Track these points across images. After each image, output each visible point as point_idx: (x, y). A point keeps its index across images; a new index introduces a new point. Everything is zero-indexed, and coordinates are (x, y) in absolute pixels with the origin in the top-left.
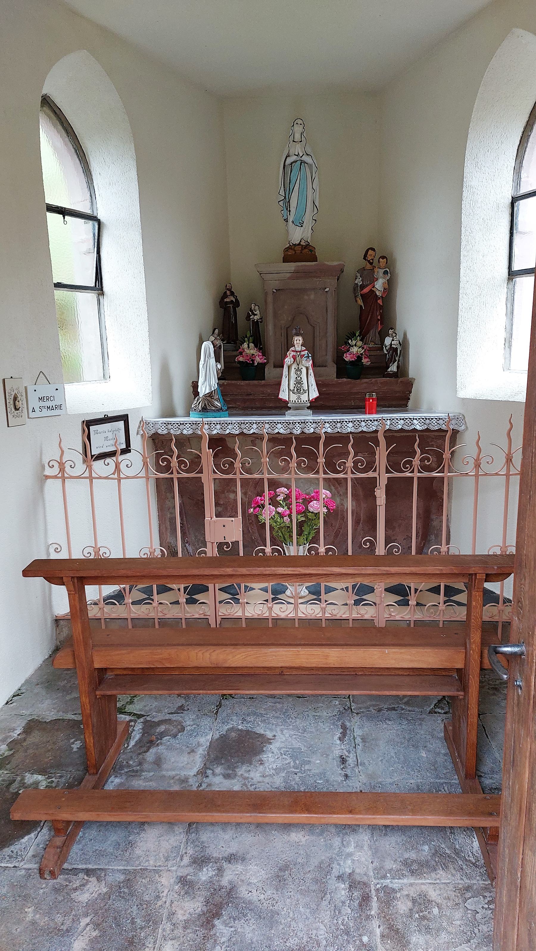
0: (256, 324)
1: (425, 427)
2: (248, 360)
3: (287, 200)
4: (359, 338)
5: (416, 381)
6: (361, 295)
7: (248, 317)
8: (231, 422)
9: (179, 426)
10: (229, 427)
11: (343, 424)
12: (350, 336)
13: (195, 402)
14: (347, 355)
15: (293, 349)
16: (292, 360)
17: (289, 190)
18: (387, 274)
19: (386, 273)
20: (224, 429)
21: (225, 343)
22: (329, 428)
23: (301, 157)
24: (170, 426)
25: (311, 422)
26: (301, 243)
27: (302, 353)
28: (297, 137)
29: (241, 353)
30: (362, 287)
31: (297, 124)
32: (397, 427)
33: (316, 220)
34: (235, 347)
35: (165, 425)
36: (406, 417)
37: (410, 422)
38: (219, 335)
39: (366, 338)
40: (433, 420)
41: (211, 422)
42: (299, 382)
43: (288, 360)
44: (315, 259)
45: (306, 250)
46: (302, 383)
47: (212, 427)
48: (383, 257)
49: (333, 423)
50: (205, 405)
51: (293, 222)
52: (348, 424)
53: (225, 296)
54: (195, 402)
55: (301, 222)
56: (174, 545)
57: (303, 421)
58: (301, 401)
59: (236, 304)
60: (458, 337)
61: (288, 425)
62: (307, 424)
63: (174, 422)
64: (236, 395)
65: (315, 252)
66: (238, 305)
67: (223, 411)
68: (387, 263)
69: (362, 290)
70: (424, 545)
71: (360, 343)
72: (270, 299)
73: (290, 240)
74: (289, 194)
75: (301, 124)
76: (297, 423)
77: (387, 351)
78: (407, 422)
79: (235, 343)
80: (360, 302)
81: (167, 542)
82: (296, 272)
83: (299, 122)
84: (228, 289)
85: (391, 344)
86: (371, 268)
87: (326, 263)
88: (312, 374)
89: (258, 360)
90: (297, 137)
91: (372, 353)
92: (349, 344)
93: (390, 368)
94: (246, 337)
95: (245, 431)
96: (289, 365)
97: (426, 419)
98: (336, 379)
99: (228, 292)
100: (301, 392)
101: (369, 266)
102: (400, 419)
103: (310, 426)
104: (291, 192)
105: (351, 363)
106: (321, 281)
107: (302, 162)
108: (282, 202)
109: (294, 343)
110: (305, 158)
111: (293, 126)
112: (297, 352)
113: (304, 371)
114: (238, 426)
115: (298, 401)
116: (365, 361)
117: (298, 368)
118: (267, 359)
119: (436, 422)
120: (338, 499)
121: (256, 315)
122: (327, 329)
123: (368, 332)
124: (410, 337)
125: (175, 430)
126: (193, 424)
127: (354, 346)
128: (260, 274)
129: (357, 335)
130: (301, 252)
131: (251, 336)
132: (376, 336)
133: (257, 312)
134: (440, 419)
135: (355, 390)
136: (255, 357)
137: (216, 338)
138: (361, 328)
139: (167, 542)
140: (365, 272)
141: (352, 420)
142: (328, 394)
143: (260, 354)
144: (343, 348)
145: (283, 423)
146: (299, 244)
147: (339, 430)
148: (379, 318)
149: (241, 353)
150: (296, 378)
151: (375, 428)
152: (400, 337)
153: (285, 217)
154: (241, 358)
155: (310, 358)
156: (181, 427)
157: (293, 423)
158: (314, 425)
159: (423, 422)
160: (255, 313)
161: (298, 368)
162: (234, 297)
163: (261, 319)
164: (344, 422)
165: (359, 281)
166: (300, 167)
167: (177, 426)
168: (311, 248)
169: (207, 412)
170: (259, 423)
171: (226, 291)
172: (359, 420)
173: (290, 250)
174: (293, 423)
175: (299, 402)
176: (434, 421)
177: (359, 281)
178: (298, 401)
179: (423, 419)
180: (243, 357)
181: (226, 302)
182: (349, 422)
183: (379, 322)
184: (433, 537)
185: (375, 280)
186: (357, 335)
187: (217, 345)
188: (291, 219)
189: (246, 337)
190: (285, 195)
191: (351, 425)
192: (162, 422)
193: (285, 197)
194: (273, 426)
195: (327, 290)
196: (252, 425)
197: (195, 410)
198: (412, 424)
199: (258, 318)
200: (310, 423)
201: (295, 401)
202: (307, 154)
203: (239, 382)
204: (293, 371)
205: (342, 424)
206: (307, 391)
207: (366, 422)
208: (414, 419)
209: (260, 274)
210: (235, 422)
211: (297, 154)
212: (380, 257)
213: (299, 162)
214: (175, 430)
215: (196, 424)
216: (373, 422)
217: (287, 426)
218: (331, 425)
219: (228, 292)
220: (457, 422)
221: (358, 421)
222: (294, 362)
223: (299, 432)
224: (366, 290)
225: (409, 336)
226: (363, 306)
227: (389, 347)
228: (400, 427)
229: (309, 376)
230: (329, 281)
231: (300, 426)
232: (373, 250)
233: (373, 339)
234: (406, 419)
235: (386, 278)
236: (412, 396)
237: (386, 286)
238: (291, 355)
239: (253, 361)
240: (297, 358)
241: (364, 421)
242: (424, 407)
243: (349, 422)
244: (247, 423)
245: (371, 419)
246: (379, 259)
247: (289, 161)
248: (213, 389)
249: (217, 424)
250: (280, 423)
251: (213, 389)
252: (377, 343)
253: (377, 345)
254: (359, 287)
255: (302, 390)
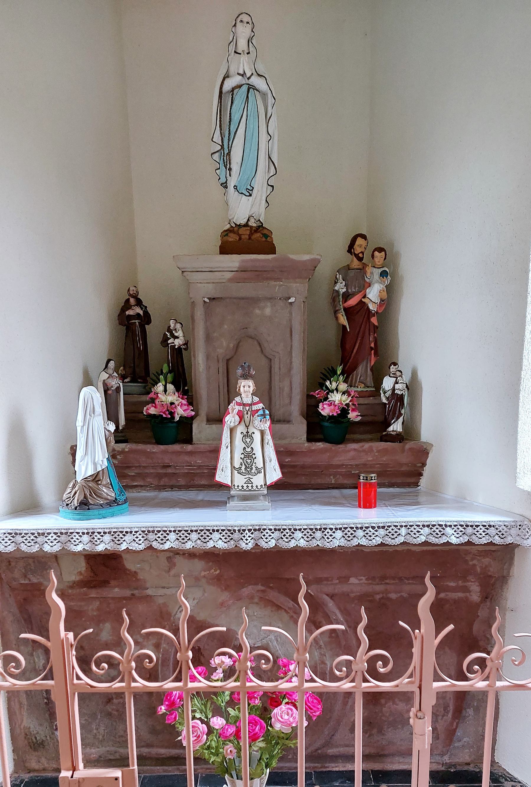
0: (178, 352)
1: (465, 539)
2: (164, 413)
3: (226, 151)
4: (341, 378)
5: (434, 448)
6: (345, 309)
7: (165, 340)
8: (129, 530)
9: (36, 537)
10: (125, 538)
11: (326, 533)
12: (328, 375)
13: (69, 490)
14: (325, 406)
15: (238, 399)
16: (237, 418)
17: (229, 134)
18: (387, 277)
19: (384, 274)
20: (117, 542)
21: (128, 382)
22: (302, 540)
23: (249, 78)
24: (19, 539)
25: (270, 530)
26: (250, 224)
27: (255, 408)
28: (242, 45)
29: (153, 401)
30: (347, 296)
31: (241, 21)
32: (418, 539)
33: (272, 186)
34: (145, 387)
35: (9, 537)
36: (433, 523)
37: (440, 531)
38: (116, 370)
39: (352, 378)
40: (479, 528)
41: (95, 530)
42: (248, 456)
43: (231, 419)
44: (272, 250)
45: (258, 235)
46: (254, 456)
47: (96, 538)
48: (380, 250)
49: (309, 531)
50: (85, 497)
51: (235, 187)
52: (334, 532)
53: (127, 305)
54: (69, 490)
55: (249, 187)
56: (35, 732)
57: (257, 528)
58: (252, 487)
59: (146, 318)
60: (521, 388)
61: (232, 534)
62: (265, 533)
63: (27, 532)
64: (145, 467)
65: (272, 238)
66: (149, 322)
67: (118, 505)
68: (385, 259)
69: (345, 302)
70: (457, 724)
71: (343, 387)
72: (199, 313)
73: (230, 218)
74: (229, 142)
75: (248, 23)
76: (247, 531)
77: (387, 399)
78: (434, 531)
79: (145, 381)
80: (343, 320)
81: (22, 727)
82: (242, 270)
83: (246, 18)
84: (131, 295)
85: (394, 389)
86: (360, 267)
87: (292, 256)
88: (271, 443)
89: (180, 412)
90: (242, 45)
91: (362, 401)
92: (327, 388)
93: (392, 426)
94: (162, 373)
95: (155, 545)
96: (231, 427)
97: (467, 526)
98: (306, 445)
99: (132, 301)
100: (253, 471)
101: (356, 263)
102: (424, 526)
103: (270, 536)
104: (231, 138)
105: (331, 418)
106: (282, 285)
107: (251, 87)
108: (217, 154)
109: (239, 390)
110: (255, 81)
111: (235, 25)
112: (244, 405)
113: (257, 437)
114: (143, 537)
115: (248, 487)
116: (353, 416)
117: (248, 432)
118: (196, 410)
119: (484, 532)
120: (316, 654)
121: (177, 337)
122: (291, 363)
123: (354, 368)
124: (424, 377)
125: (29, 544)
126: (62, 533)
127: (335, 392)
128: (183, 272)
129: (339, 373)
130: (250, 238)
131: (170, 372)
132: (366, 374)
133: (179, 333)
134: (490, 526)
135: (336, 461)
136: (176, 407)
137: (110, 376)
138: (344, 361)
139: (22, 727)
140: (351, 273)
141: (341, 526)
142: (294, 467)
143: (184, 402)
144: (318, 394)
145: (223, 530)
146: (246, 225)
147: (318, 543)
148: (372, 345)
149: (153, 401)
150: (244, 448)
151: (381, 540)
152: (406, 378)
153: (223, 180)
154: (153, 409)
155: (268, 417)
156: (40, 539)
157: (239, 531)
158: (277, 534)
159: (461, 531)
160: (176, 334)
161: (248, 432)
162: (142, 309)
163: (186, 344)
164: (328, 530)
165: (341, 287)
166: (247, 97)
167: (32, 537)
168: (265, 232)
169: (89, 509)
170: (180, 531)
171: (129, 299)
172: (353, 526)
173: (231, 235)
174: (239, 531)
175: (250, 488)
176: (481, 530)
177: (341, 287)
178: (248, 487)
179: (462, 526)
180: (155, 407)
181: (129, 315)
182: (336, 529)
183: (373, 351)
184: (470, 712)
185: (366, 285)
186: (339, 373)
187: (112, 387)
188: (231, 184)
189: (162, 373)
190: (222, 142)
191: (339, 534)
192: (4, 531)
193: (222, 146)
194: (205, 536)
195: (292, 300)
196: (168, 534)
197: (67, 505)
198: (443, 534)
199: (181, 343)
200: (268, 531)
201: (243, 487)
202: (259, 75)
203: (149, 448)
204: (238, 437)
205: (323, 532)
206: (263, 471)
207: (364, 531)
208: (446, 526)
209: (183, 272)
210: (137, 530)
211: (242, 73)
212: (375, 250)
213: (245, 88)
214: (29, 544)
215: (66, 533)
216: (376, 531)
217: (229, 536)
218: (305, 535)
219: (132, 301)
220: (519, 532)
221: (352, 528)
222: (240, 422)
223: (250, 546)
224: (352, 302)
225: (422, 376)
226: (348, 327)
227: (389, 393)
228: (423, 539)
229: (266, 446)
230: (295, 285)
231: (252, 536)
232: (364, 237)
233: (362, 378)
234: (434, 526)
235: (384, 282)
236: (426, 471)
237: (385, 295)
238: (236, 411)
239: (172, 414)
240: (246, 416)
241: (361, 528)
242: (450, 492)
243: (336, 529)
244: (159, 531)
245: (374, 525)
246: (373, 252)
247: (229, 85)
248: (100, 469)
249: (105, 533)
250: (218, 531)
251: (99, 469)
252: (369, 384)
253: (368, 387)
254: (341, 297)
255: (254, 469)
